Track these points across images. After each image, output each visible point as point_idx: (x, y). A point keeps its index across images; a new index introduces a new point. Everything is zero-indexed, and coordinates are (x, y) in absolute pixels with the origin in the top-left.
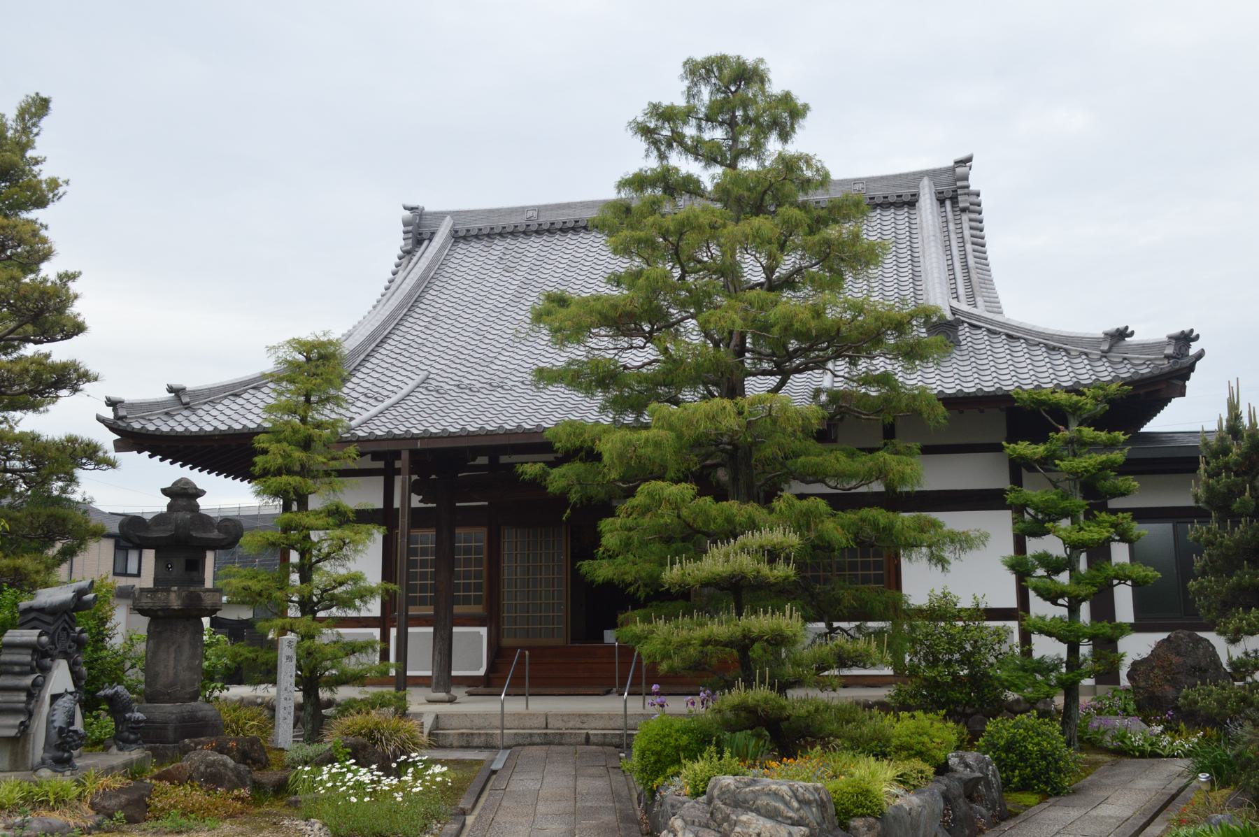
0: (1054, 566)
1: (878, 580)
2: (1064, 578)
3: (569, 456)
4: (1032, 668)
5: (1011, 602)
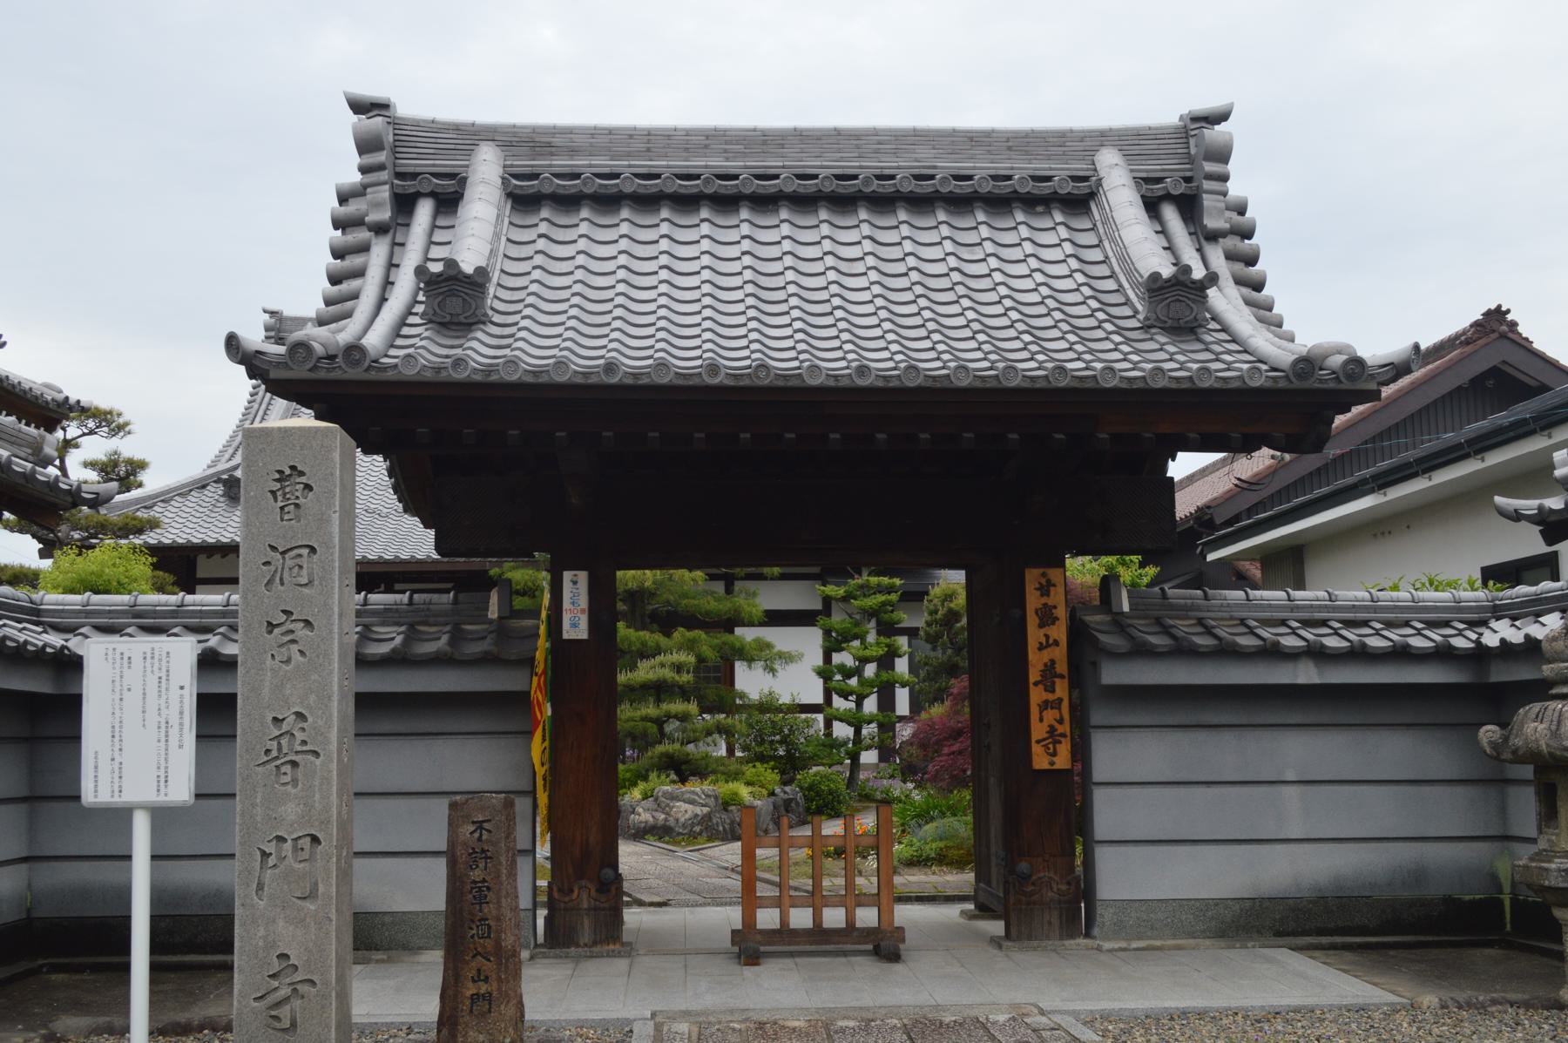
0: (847, 673)
1: (717, 680)
2: (854, 682)
3: (523, 593)
4: (831, 744)
5: (819, 699)
